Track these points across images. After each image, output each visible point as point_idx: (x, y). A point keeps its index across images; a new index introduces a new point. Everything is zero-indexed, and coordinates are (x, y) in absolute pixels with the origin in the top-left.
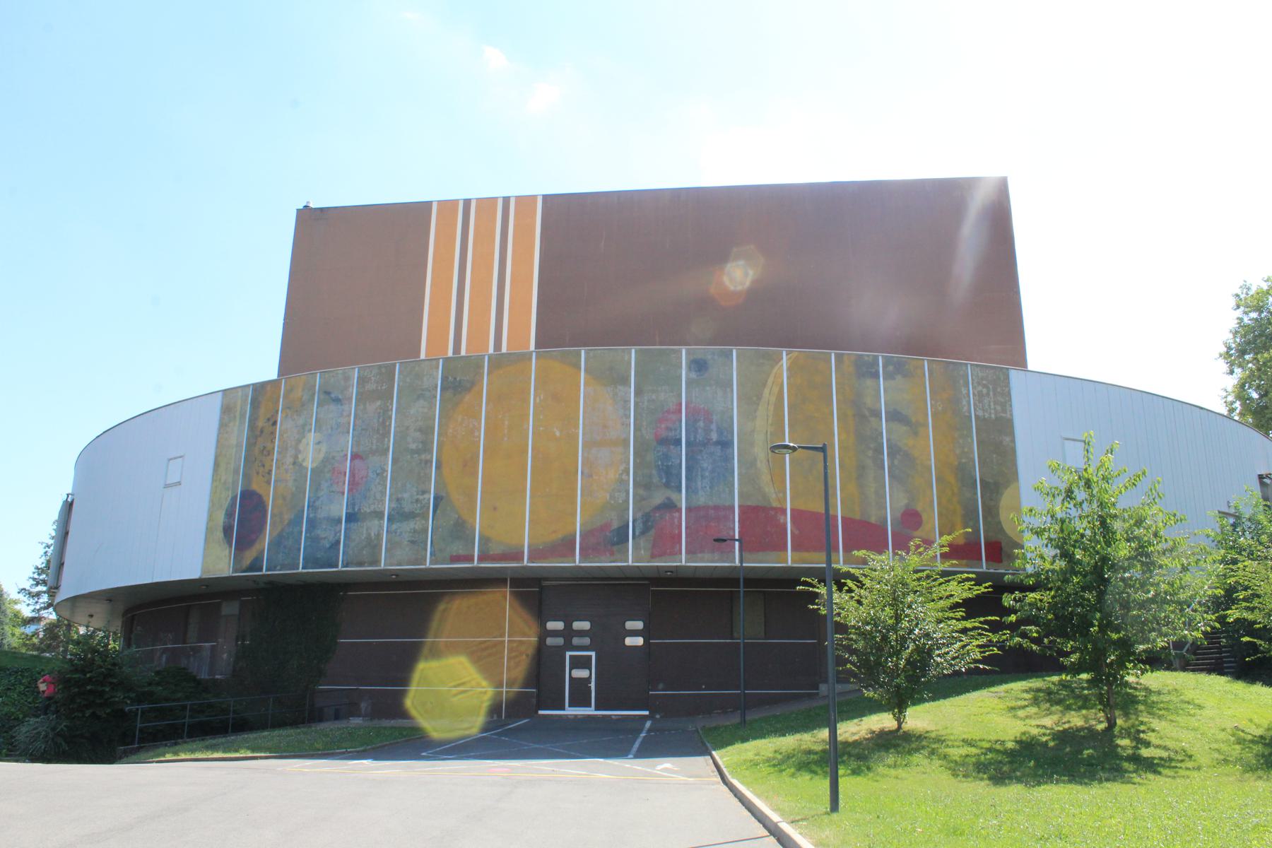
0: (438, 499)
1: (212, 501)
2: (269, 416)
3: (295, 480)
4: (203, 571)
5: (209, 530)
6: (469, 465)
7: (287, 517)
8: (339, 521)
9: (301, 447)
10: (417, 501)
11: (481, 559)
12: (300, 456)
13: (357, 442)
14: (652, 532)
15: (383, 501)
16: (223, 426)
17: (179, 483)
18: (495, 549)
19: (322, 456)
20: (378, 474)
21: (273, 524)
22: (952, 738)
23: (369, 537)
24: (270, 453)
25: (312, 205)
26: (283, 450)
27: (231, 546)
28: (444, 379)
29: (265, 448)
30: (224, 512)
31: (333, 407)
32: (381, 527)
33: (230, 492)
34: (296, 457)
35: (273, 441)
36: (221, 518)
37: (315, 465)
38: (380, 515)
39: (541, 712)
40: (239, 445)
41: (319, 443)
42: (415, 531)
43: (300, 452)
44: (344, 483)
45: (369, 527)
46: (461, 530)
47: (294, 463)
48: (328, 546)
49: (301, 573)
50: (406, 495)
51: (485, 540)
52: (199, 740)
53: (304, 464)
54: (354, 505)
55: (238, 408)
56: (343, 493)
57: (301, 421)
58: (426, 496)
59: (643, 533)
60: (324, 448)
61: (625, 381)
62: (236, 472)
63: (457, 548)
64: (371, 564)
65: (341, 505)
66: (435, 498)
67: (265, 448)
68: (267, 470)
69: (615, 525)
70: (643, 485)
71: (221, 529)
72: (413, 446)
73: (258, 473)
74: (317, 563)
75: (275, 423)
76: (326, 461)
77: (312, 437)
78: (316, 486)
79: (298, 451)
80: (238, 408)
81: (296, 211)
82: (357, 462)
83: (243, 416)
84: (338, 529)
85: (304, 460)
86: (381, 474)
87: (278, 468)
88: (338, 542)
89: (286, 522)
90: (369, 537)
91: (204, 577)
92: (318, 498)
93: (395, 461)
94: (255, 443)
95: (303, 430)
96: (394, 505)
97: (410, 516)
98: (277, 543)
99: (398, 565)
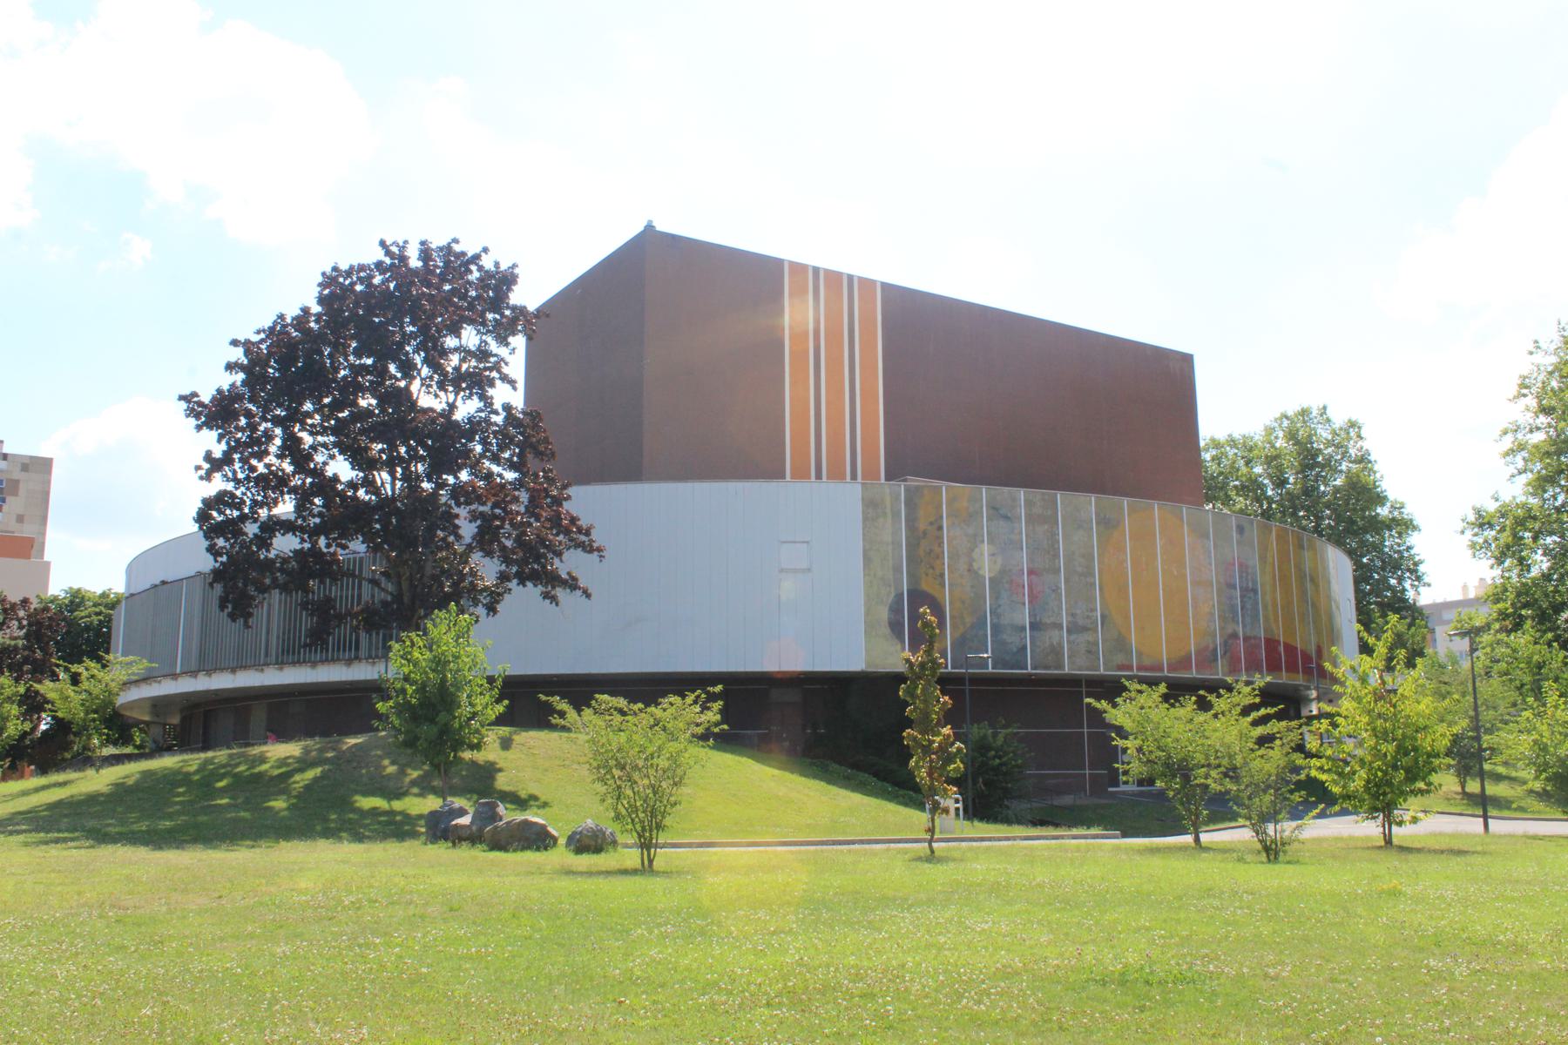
0: (1103, 616)
1: (867, 595)
2: (932, 519)
3: (972, 587)
4: (868, 664)
5: (870, 627)
6: (1123, 591)
7: (968, 620)
8: (1024, 628)
9: (975, 555)
10: (1088, 617)
11: (1139, 669)
12: (974, 564)
13: (1030, 560)
14: (1228, 654)
15: (1060, 614)
16: (868, 521)
17: (809, 570)
18: (1147, 662)
19: (998, 567)
20: (1053, 591)
21: (954, 626)
22: (21, 838)
23: (1052, 645)
24: (940, 556)
25: (661, 226)
26: (954, 556)
27: (903, 642)
28: (1097, 514)
29: (931, 551)
30: (887, 609)
31: (1002, 523)
32: (1062, 637)
33: (893, 589)
34: (971, 565)
35: (941, 544)
36: (884, 614)
37: (992, 575)
38: (1060, 627)
39: (1110, 789)
40: (896, 544)
41: (993, 555)
42: (1089, 642)
43: (974, 560)
44: (1024, 595)
45: (1052, 637)
46: (1121, 644)
47: (969, 570)
48: (1015, 650)
49: (1030, 675)
50: (1078, 612)
51: (1139, 654)
52: (247, 847)
53: (981, 572)
54: (1035, 615)
55: (888, 504)
56: (1024, 604)
57: (971, 531)
58: (1094, 614)
59: (1225, 653)
60: (999, 560)
61: (1208, 538)
62: (898, 569)
63: (1119, 659)
64: (1056, 668)
65: (1024, 614)
66: (1102, 616)
67: (931, 551)
68: (938, 572)
69: (1211, 646)
70: (1222, 618)
71: (887, 624)
72: (1079, 569)
73: (927, 575)
74: (1006, 665)
75: (940, 528)
76: (1003, 572)
77: (985, 547)
78: (996, 596)
79: (971, 561)
80: (888, 504)
81: (638, 228)
82: (1033, 577)
83: (896, 514)
84: (1023, 636)
85: (979, 569)
86: (1056, 590)
87: (950, 572)
88: (1025, 648)
89: (968, 625)
90: (1052, 645)
91: (870, 670)
92: (1000, 606)
93: (1067, 581)
94: (918, 544)
95: (975, 540)
96: (1070, 619)
97: (1085, 629)
98: (959, 644)
99: (1087, 669)
